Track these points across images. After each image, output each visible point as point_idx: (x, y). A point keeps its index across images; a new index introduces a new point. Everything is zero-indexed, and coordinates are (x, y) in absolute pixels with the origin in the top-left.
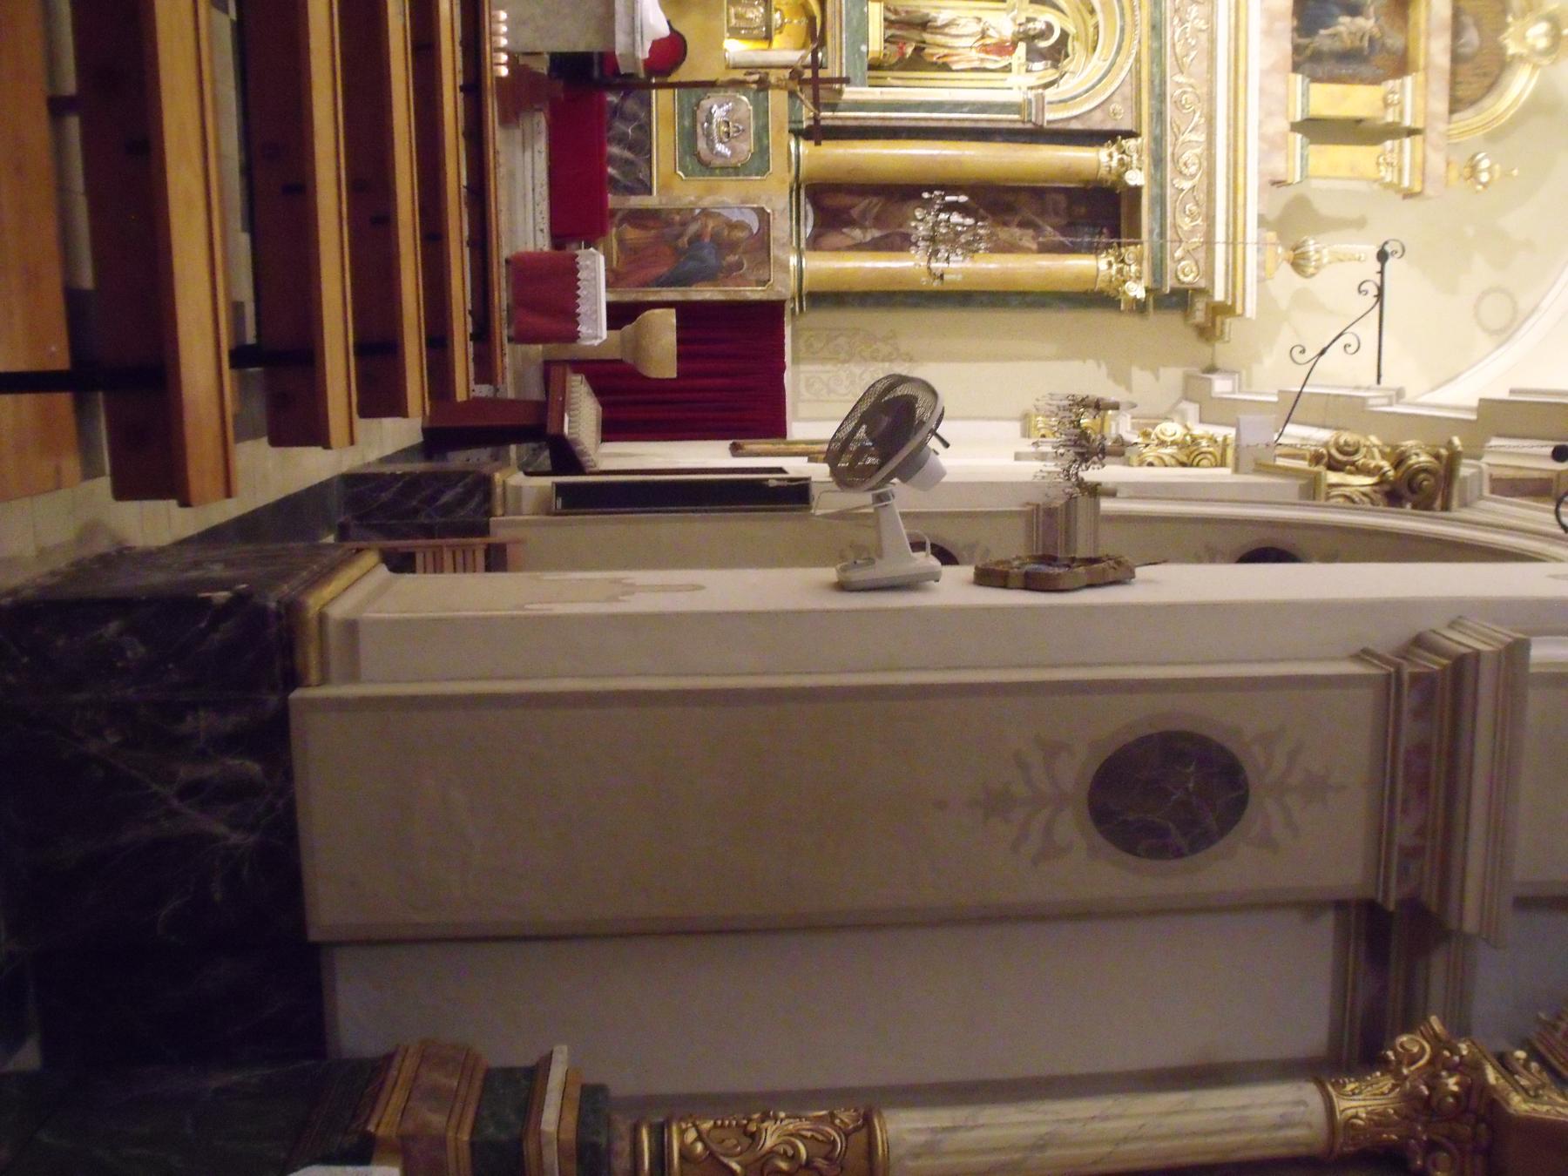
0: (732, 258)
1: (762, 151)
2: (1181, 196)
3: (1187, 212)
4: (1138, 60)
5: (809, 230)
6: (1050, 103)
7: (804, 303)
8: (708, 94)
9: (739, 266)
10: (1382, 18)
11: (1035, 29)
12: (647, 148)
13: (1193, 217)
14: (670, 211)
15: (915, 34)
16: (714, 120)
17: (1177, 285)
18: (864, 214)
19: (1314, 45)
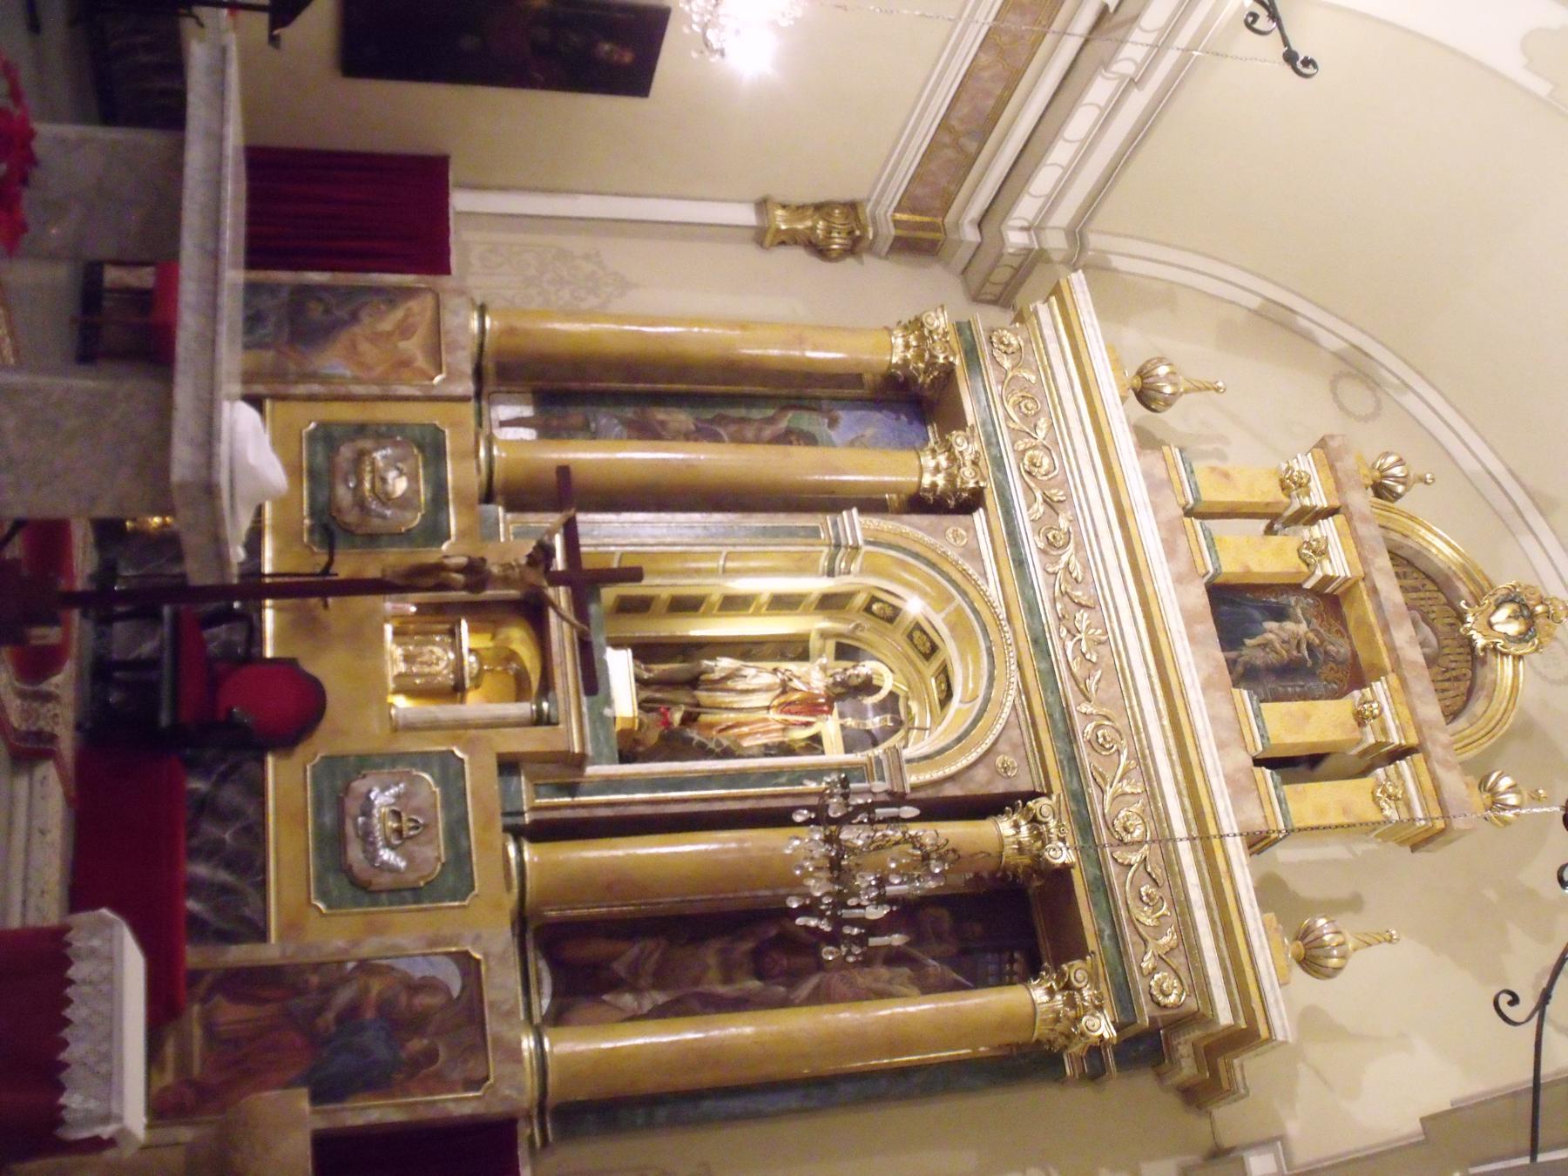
0: (417, 1045)
1: (460, 859)
2: (1130, 875)
3: (1145, 898)
4: (1025, 690)
5: (546, 1002)
6: (909, 761)
7: (549, 1126)
8: (363, 772)
9: (431, 1056)
10: (1314, 621)
11: (858, 676)
12: (258, 864)
13: (1154, 905)
14: (299, 969)
15: (683, 696)
16: (375, 812)
17: (1158, 1013)
18: (635, 968)
19: (1246, 658)
